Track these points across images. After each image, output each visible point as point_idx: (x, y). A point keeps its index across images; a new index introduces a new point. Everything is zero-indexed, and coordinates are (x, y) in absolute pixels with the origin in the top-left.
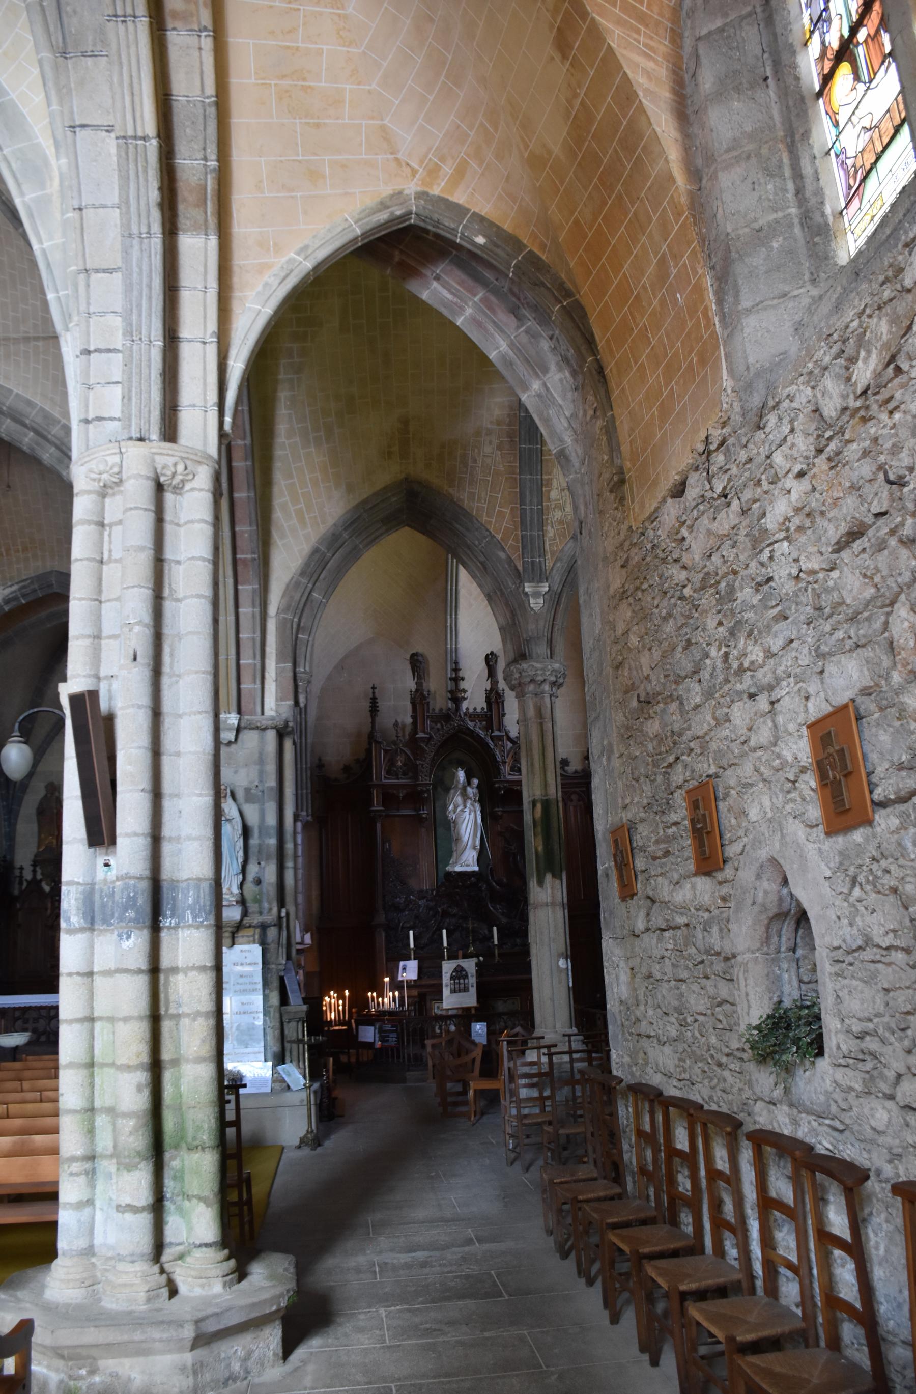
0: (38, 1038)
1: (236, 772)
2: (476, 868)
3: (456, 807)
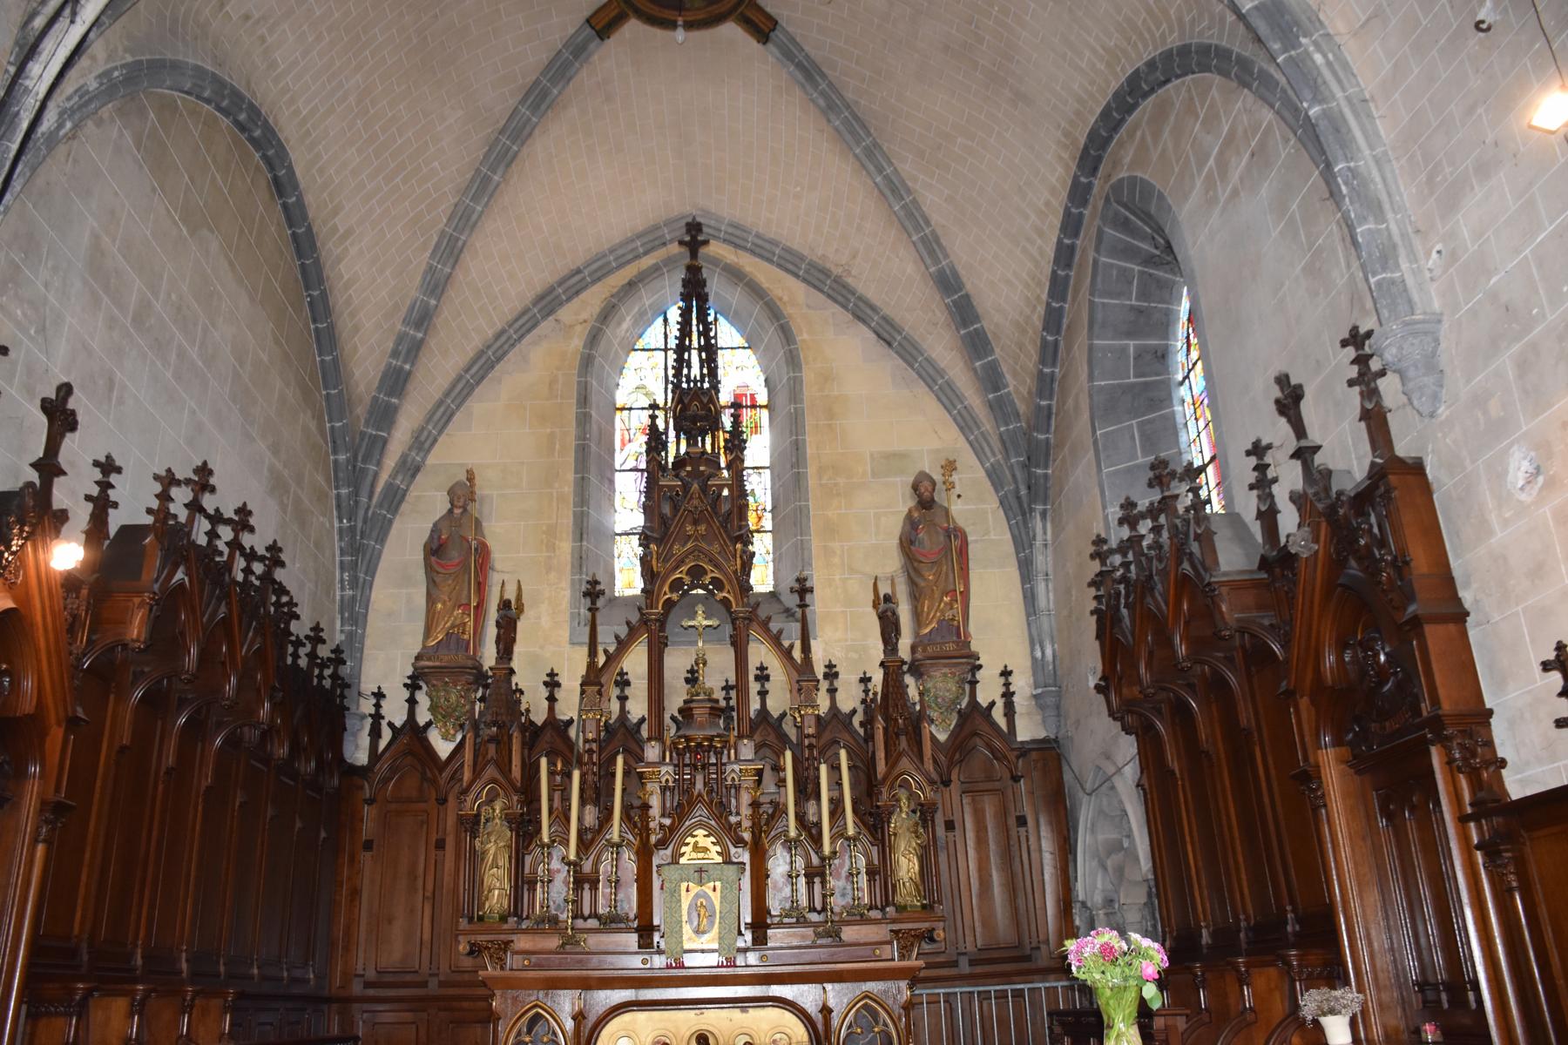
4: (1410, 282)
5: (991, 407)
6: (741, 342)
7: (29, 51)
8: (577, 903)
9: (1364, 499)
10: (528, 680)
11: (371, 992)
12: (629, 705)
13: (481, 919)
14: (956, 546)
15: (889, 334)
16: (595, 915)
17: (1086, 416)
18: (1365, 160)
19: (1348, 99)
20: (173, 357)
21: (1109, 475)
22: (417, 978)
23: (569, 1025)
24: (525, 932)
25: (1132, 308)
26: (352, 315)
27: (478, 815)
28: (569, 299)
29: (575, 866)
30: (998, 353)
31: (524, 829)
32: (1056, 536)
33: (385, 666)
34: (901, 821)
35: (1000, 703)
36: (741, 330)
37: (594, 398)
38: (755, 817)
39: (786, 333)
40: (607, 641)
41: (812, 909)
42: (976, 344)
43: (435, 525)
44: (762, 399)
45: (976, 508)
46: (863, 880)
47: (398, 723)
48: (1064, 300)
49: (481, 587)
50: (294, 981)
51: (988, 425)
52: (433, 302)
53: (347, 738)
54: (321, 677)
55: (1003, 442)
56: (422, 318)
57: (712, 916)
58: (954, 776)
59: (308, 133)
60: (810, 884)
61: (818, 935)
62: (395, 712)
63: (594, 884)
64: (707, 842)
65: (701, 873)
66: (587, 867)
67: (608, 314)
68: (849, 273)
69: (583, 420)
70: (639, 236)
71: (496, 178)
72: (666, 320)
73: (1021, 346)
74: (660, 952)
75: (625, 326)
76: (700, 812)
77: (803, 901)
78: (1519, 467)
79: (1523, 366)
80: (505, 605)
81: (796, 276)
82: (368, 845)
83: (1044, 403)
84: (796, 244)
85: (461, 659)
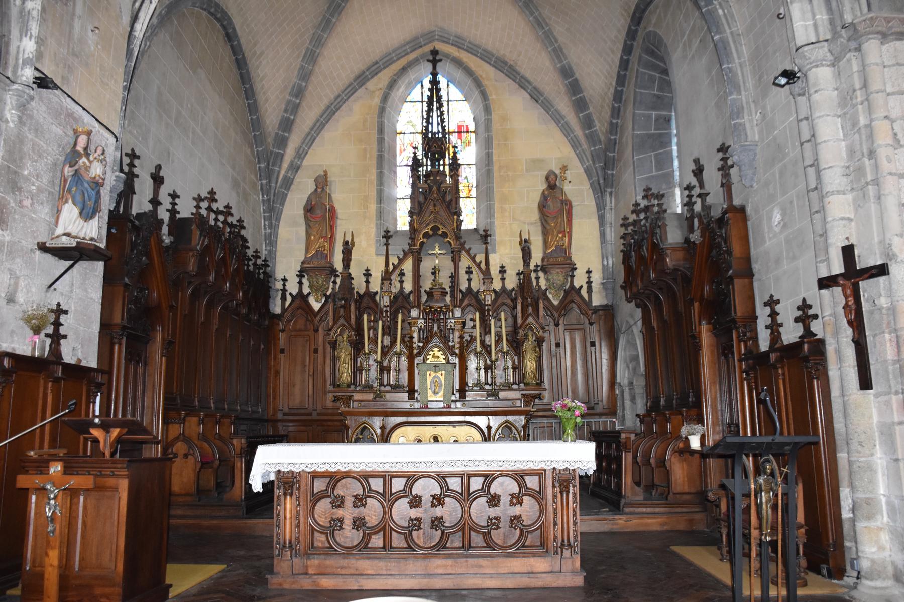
0: (366, 538)
4: (748, 126)
5: (587, 137)
7: (135, 18)
8: (381, 380)
9: (721, 221)
10: (356, 271)
11: (286, 418)
12: (405, 285)
13: (339, 386)
14: (566, 209)
15: (537, 96)
17: (630, 148)
18: (735, 65)
19: (732, 33)
20: (191, 135)
21: (639, 180)
22: (307, 412)
23: (379, 431)
24: (358, 392)
25: (655, 95)
26: (264, 93)
27: (336, 341)
28: (372, 77)
29: (380, 363)
30: (591, 109)
31: (357, 347)
32: (616, 205)
33: (287, 267)
34: (528, 345)
36: (462, 91)
37: (386, 130)
38: (461, 342)
39: (484, 95)
40: (394, 260)
41: (487, 384)
42: (580, 105)
43: (309, 198)
44: (472, 128)
45: (578, 190)
46: (510, 371)
47: (294, 293)
48: (623, 86)
49: (332, 228)
50: (253, 412)
51: (585, 146)
52: (304, 84)
53: (271, 300)
54: (259, 274)
55: (592, 156)
56: (299, 93)
57: (441, 386)
58: (561, 322)
59: (241, 9)
60: (486, 372)
61: (488, 395)
63: (389, 371)
64: (439, 354)
65: (436, 368)
66: (385, 363)
67: (392, 85)
68: (516, 63)
69: (381, 141)
70: (408, 43)
71: (334, 20)
72: (422, 86)
73: (602, 107)
74: (418, 401)
75: (401, 90)
76: (436, 340)
77: (483, 380)
78: (777, 217)
79: (782, 173)
80: (346, 243)
81: (490, 64)
82: (282, 351)
83: (612, 138)
84: (489, 47)
85: (323, 264)
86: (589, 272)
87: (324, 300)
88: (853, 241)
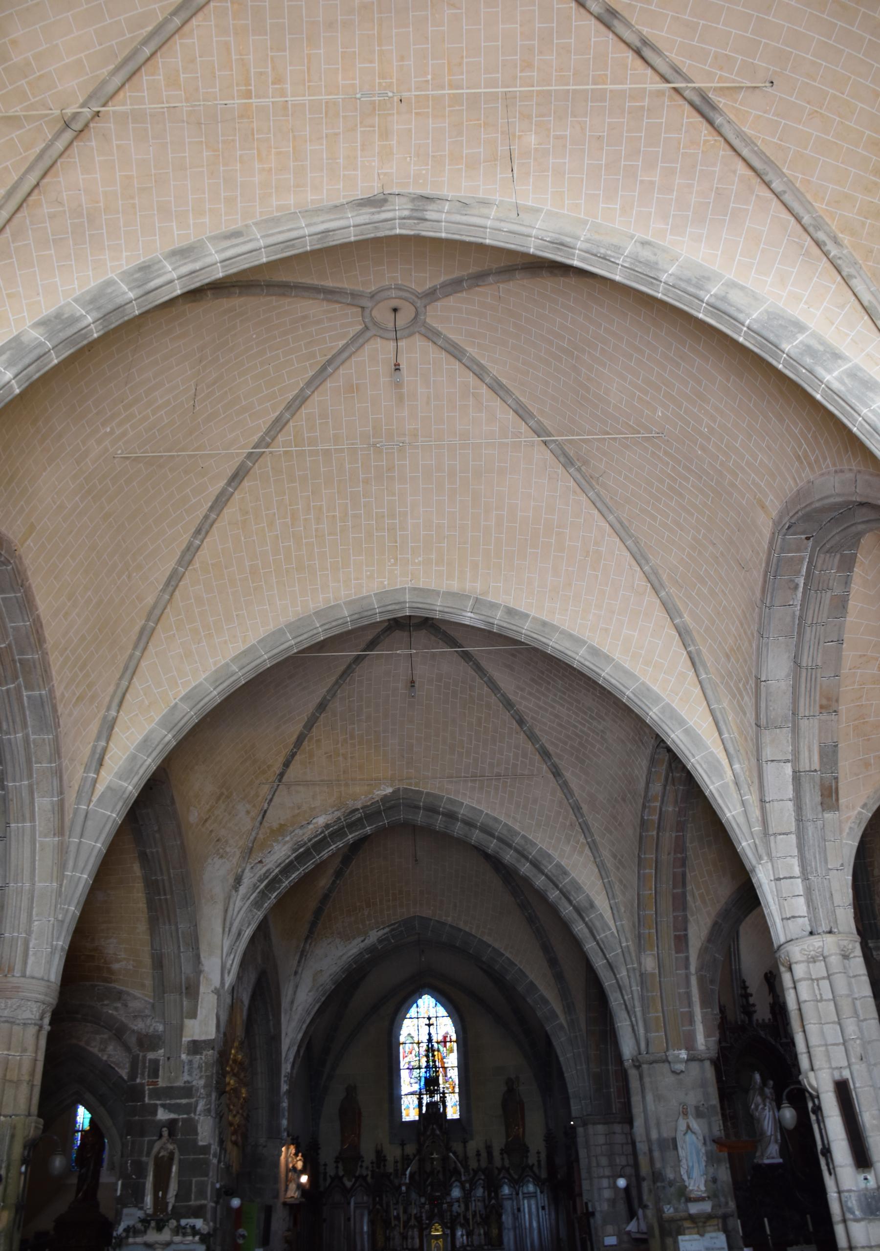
1: (686, 1094)
2: (781, 1160)
3: (757, 1106)
6: (446, 1014)
16: (407, 1248)
35: (536, 1164)
44: (454, 1038)
46: (483, 1237)
62: (331, 1171)
63: (407, 1239)
86: (538, 1153)
87: (353, 1180)
88: (846, 1074)
